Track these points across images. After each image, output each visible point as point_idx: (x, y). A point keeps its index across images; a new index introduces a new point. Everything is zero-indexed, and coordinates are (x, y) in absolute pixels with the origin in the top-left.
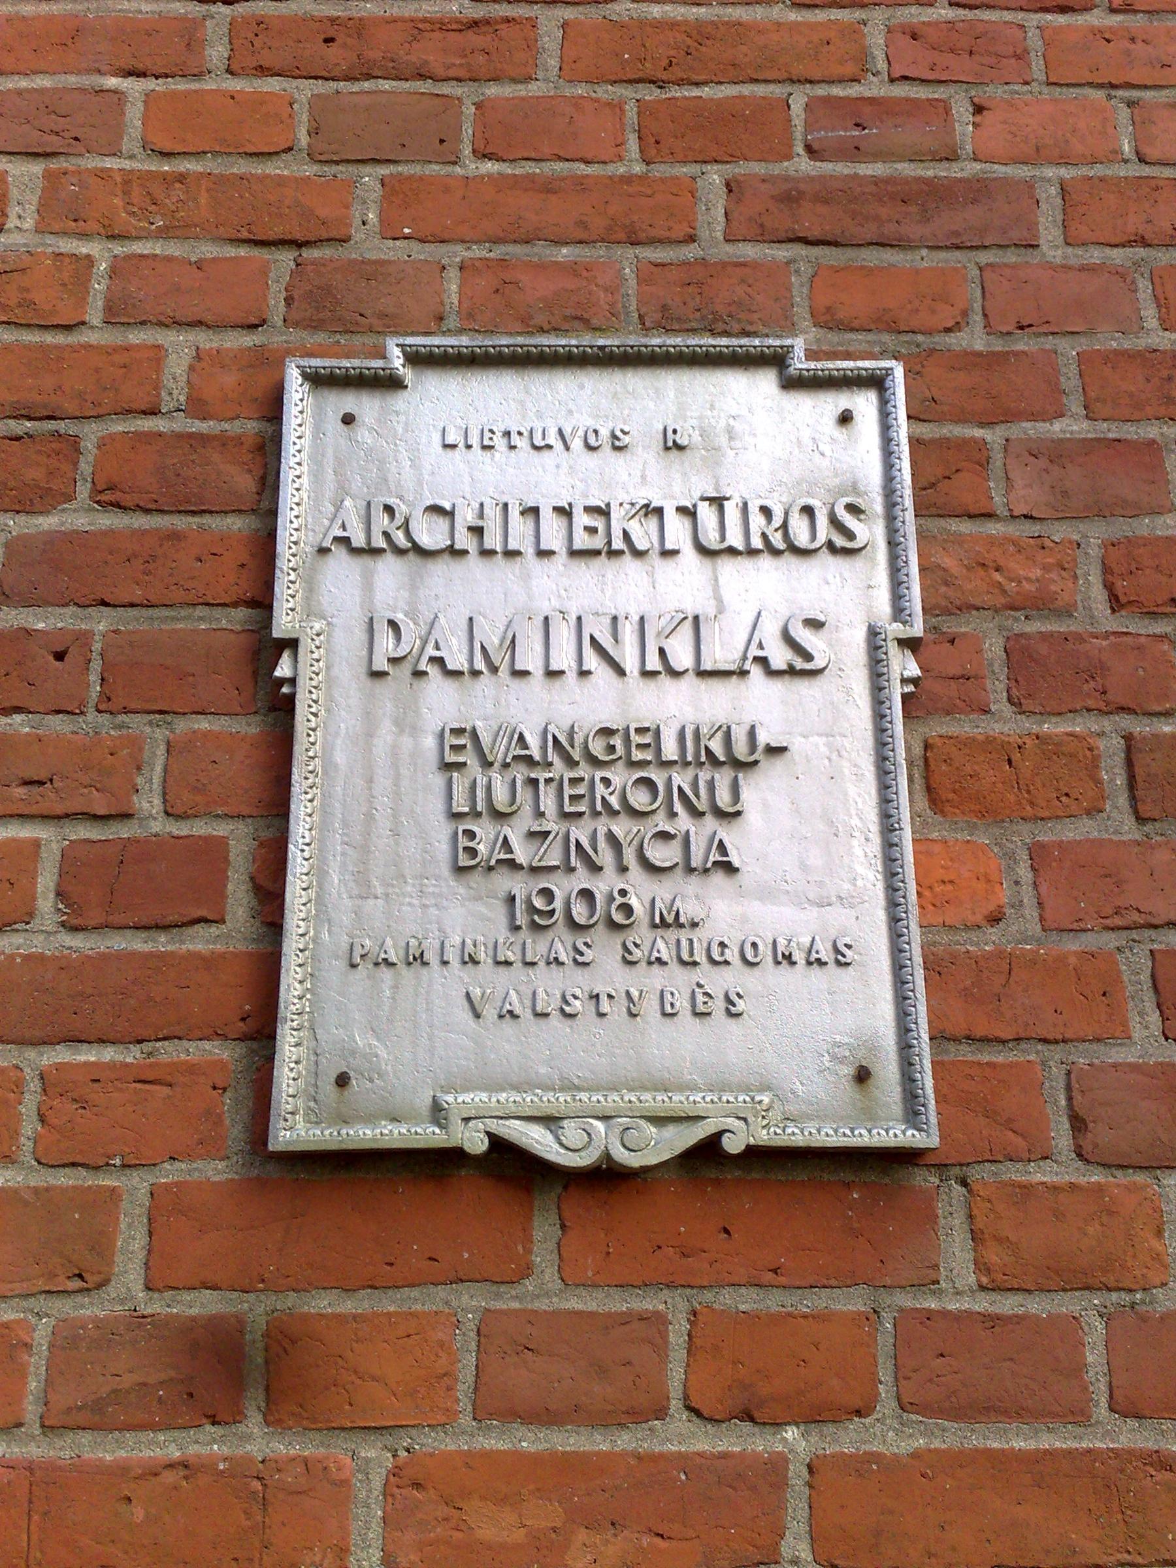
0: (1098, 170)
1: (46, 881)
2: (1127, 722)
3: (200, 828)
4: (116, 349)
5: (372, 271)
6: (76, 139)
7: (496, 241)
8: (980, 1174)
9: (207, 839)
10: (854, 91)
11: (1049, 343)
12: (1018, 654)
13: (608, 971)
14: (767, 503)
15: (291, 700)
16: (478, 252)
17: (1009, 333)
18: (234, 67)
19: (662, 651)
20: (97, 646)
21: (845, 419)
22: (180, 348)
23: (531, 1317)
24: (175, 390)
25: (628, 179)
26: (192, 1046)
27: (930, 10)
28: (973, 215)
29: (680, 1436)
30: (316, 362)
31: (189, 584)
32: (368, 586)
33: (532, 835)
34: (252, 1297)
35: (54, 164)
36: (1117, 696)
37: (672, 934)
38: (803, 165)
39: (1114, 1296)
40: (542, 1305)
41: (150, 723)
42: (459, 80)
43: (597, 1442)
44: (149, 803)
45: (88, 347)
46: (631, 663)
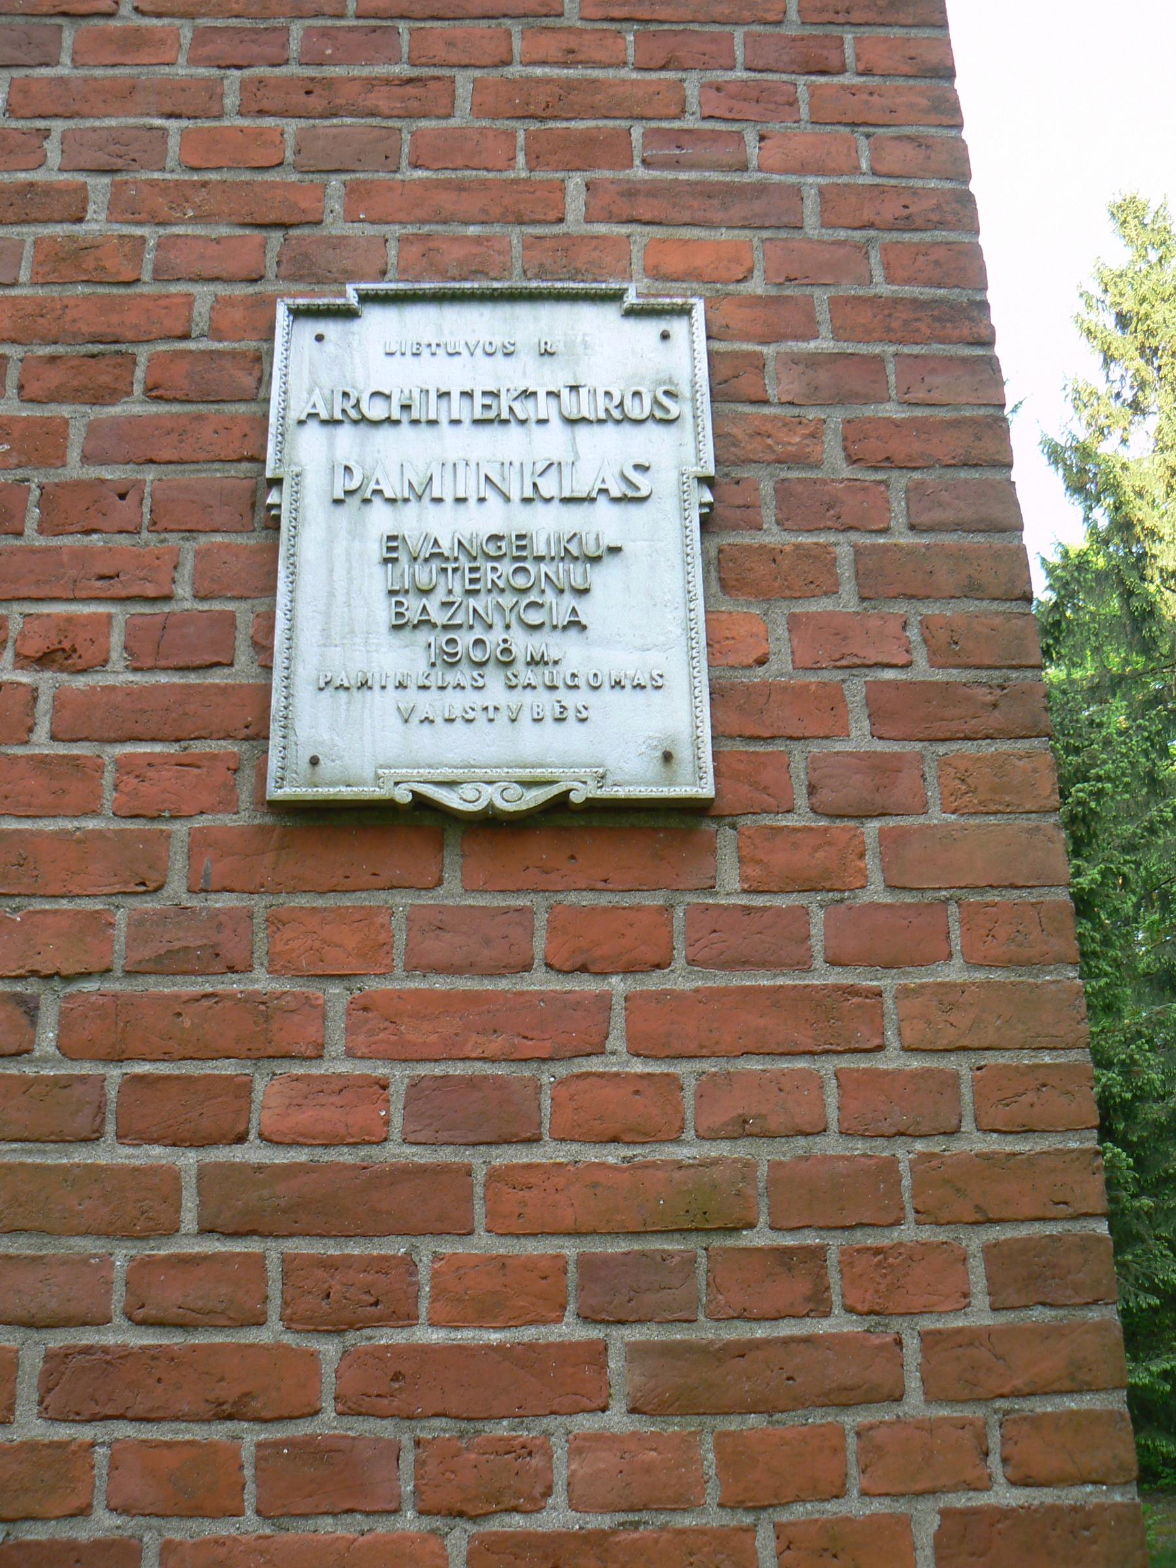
0: (844, 180)
1: (116, 639)
2: (854, 537)
3: (217, 606)
4: (160, 297)
5: (339, 243)
6: (134, 160)
7: (424, 222)
8: (747, 821)
9: (222, 612)
10: (676, 125)
11: (808, 290)
12: (783, 490)
13: (495, 690)
14: (608, 389)
15: (277, 518)
16: (410, 229)
17: (781, 284)
18: (244, 111)
19: (535, 485)
20: (147, 490)
21: (665, 336)
22: (204, 294)
23: (441, 909)
24: (201, 324)
25: (515, 182)
26: (213, 743)
27: (730, 73)
28: (758, 206)
29: (540, 982)
30: (301, 301)
31: (209, 448)
32: (331, 445)
33: (444, 604)
34: (256, 896)
35: (118, 177)
36: (847, 520)
37: (540, 669)
38: (640, 173)
39: (831, 894)
40: (450, 902)
41: (183, 539)
42: (399, 117)
43: (488, 985)
44: (183, 590)
45: (141, 295)
46: (515, 495)
